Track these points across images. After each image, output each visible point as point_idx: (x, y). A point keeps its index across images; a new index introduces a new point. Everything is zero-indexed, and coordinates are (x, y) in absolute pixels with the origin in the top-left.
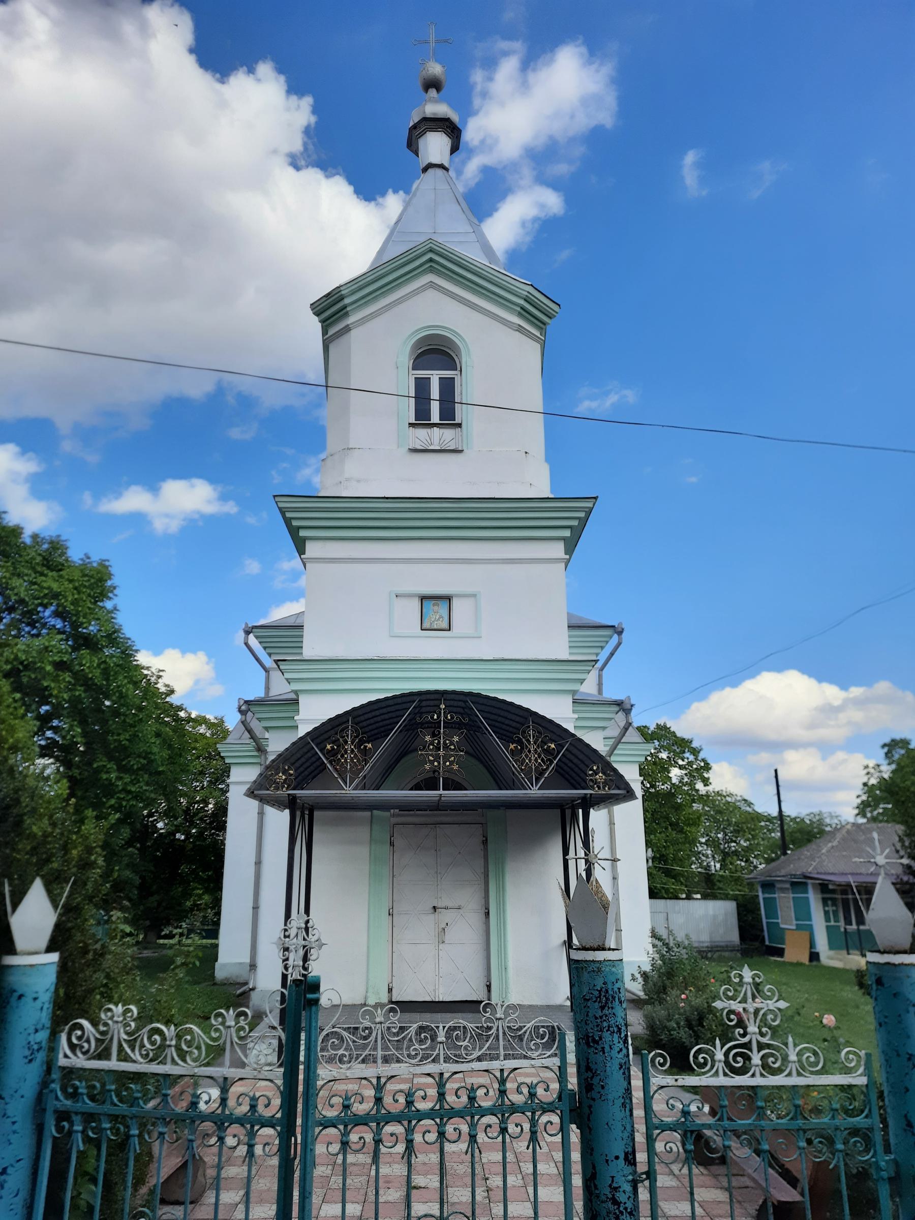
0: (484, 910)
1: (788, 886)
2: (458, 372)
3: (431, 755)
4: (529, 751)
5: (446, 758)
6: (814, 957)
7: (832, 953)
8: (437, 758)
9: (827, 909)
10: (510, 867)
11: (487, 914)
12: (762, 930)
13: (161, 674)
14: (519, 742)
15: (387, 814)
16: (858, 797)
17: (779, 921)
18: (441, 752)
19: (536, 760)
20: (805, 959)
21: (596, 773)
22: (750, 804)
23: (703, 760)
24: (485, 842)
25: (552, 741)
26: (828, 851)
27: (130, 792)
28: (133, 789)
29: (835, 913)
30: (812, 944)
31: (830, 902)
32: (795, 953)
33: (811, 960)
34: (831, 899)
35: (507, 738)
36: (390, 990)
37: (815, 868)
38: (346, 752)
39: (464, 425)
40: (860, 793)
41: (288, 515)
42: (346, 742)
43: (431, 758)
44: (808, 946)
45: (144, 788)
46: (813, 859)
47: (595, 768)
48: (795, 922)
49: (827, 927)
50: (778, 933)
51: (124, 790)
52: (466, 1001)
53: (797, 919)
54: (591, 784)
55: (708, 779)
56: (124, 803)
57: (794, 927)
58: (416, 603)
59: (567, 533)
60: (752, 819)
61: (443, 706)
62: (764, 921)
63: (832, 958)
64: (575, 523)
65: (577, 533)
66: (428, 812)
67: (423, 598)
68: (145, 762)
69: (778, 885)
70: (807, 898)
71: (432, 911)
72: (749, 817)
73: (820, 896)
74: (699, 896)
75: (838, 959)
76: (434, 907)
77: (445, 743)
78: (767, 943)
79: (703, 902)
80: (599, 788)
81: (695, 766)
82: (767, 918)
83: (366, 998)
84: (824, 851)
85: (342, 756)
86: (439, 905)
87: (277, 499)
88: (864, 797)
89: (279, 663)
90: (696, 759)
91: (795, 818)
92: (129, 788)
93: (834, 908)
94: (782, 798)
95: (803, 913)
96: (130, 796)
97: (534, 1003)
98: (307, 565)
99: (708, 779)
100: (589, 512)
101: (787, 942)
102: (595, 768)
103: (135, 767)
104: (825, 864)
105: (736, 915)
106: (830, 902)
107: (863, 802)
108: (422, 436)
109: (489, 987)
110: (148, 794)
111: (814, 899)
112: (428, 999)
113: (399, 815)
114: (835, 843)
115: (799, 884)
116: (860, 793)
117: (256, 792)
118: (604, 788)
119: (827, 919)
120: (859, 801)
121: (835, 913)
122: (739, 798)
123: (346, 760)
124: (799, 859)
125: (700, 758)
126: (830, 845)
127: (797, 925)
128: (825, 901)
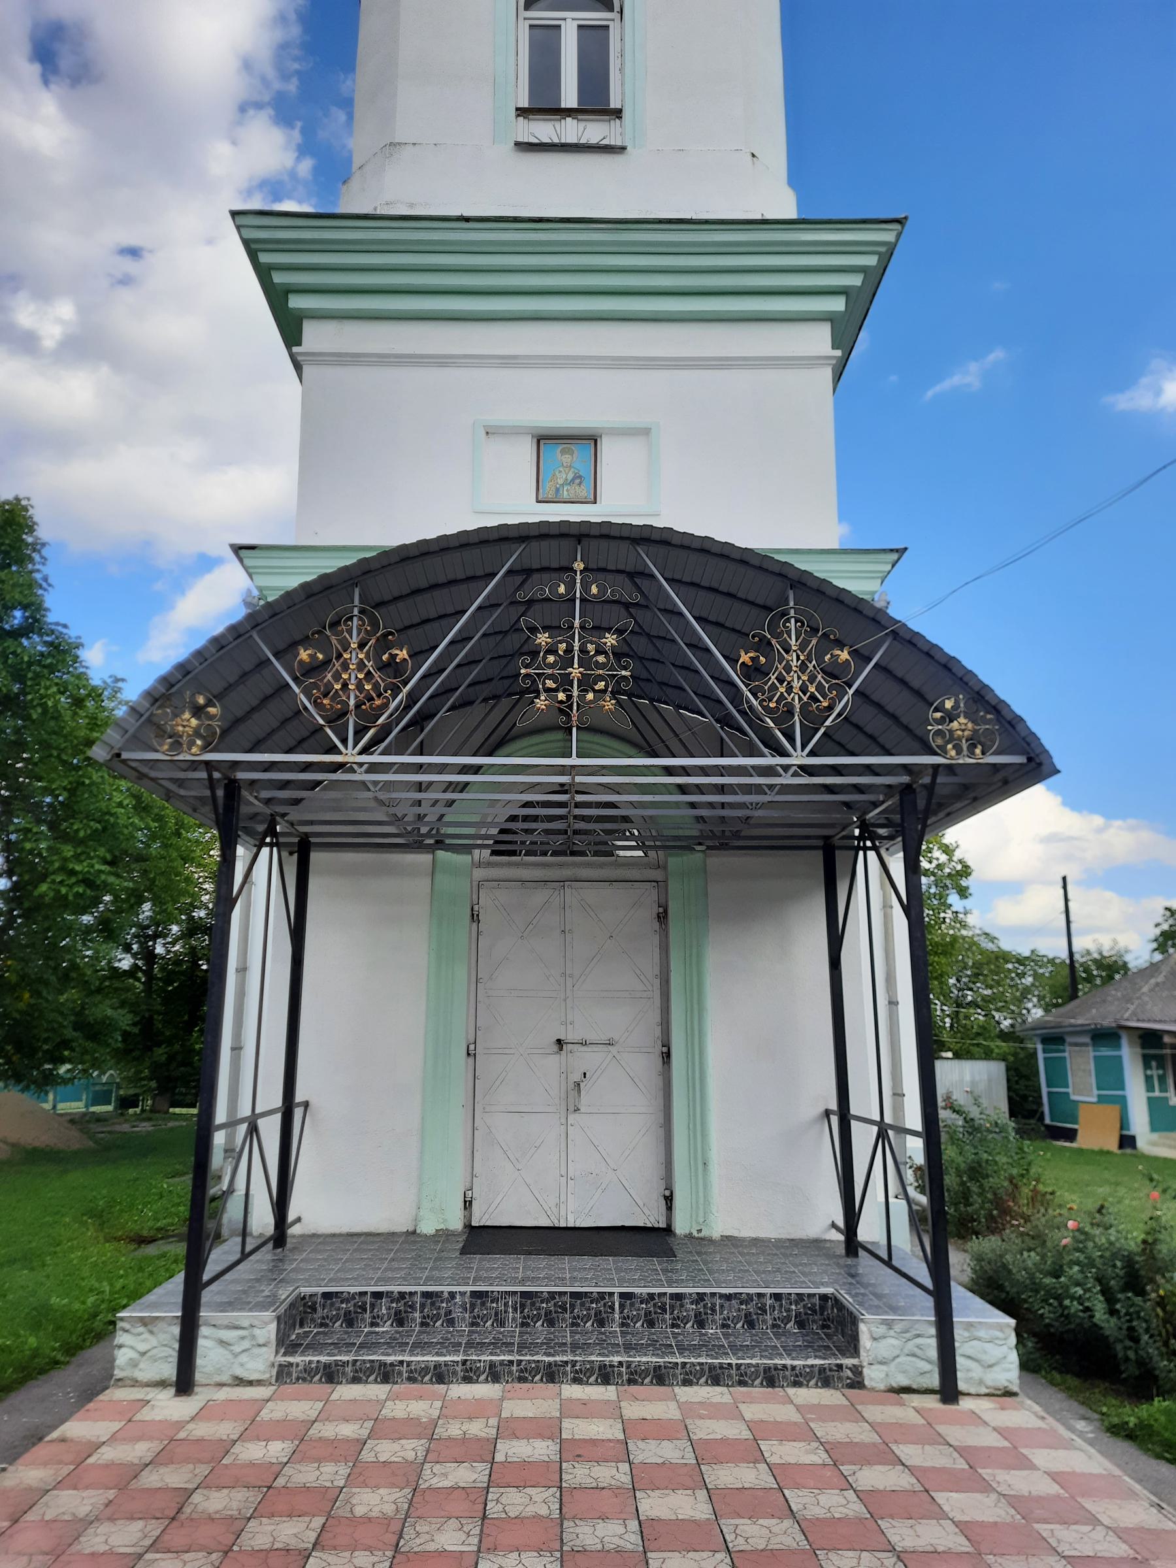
0: (659, 1048)
1: (1087, 1040)
2: (614, 15)
3: (551, 677)
4: (788, 669)
5: (586, 684)
6: (1127, 1141)
7: (1155, 1136)
8: (565, 683)
9: (1149, 1072)
10: (714, 958)
11: (667, 1056)
12: (1040, 1104)
13: (120, 684)
14: (764, 646)
15: (464, 859)
16: (1157, 925)
17: (1070, 1090)
18: (576, 672)
19: (804, 689)
20: (1112, 1145)
21: (950, 717)
22: (993, 939)
23: (960, 861)
24: (663, 917)
25: (840, 645)
26: (1151, 990)
27: (73, 873)
28: (78, 868)
29: (1162, 1079)
30: (1124, 1123)
31: (1154, 1064)
32: (1096, 1134)
33: (1121, 1146)
34: (1155, 1057)
35: (731, 635)
36: (468, 1204)
37: (1134, 1013)
38: (345, 667)
39: (626, 114)
40: (1160, 920)
41: (264, 258)
42: (346, 647)
43: (550, 684)
44: (1118, 1126)
45: (97, 867)
46: (1129, 1000)
47: (949, 704)
48: (1096, 1092)
49: (1149, 1099)
50: (1066, 1108)
51: (63, 869)
52: (623, 1228)
53: (1098, 1089)
54: (939, 741)
55: (967, 888)
56: (64, 890)
57: (1095, 1100)
58: (525, 450)
59: (838, 304)
60: (997, 958)
61: (579, 566)
62: (1044, 1090)
63: (1154, 1144)
64: (856, 280)
65: (860, 303)
66: (548, 859)
67: (544, 439)
68: (99, 826)
69: (1069, 1039)
70: (1120, 1057)
71: (556, 1048)
72: (993, 956)
73: (1139, 1050)
74: (950, 1054)
75: (1164, 1145)
76: (559, 1041)
77: (583, 651)
78: (1048, 1121)
79: (956, 1063)
80: (959, 751)
81: (947, 870)
82: (1048, 1086)
83: (416, 1220)
84: (1145, 989)
85: (337, 676)
86: (570, 1037)
87: (242, 220)
88: (1165, 927)
89: (243, 553)
90: (950, 860)
91: (1053, 959)
92: (71, 866)
93: (1161, 1072)
94: (1063, 916)
95: (1111, 1077)
96: (73, 880)
97: (762, 1234)
98: (306, 370)
99: (967, 888)
100: (887, 255)
101: (1081, 1119)
102: (949, 704)
103: (82, 834)
104: (1149, 1007)
105: (1004, 1082)
106: (1154, 1064)
107: (1163, 934)
108: (544, 130)
109: (669, 1200)
110: (103, 877)
111: (1129, 1056)
112: (544, 1222)
113: (489, 865)
114: (1160, 979)
115: (1105, 1036)
116: (1160, 920)
117: (125, 756)
118: (972, 754)
119: (1150, 1087)
120: (1158, 931)
121: (1162, 1079)
122: (978, 932)
123: (345, 685)
124: (1104, 1001)
125: (955, 859)
126: (1153, 981)
127: (1099, 1096)
128: (1147, 1061)
